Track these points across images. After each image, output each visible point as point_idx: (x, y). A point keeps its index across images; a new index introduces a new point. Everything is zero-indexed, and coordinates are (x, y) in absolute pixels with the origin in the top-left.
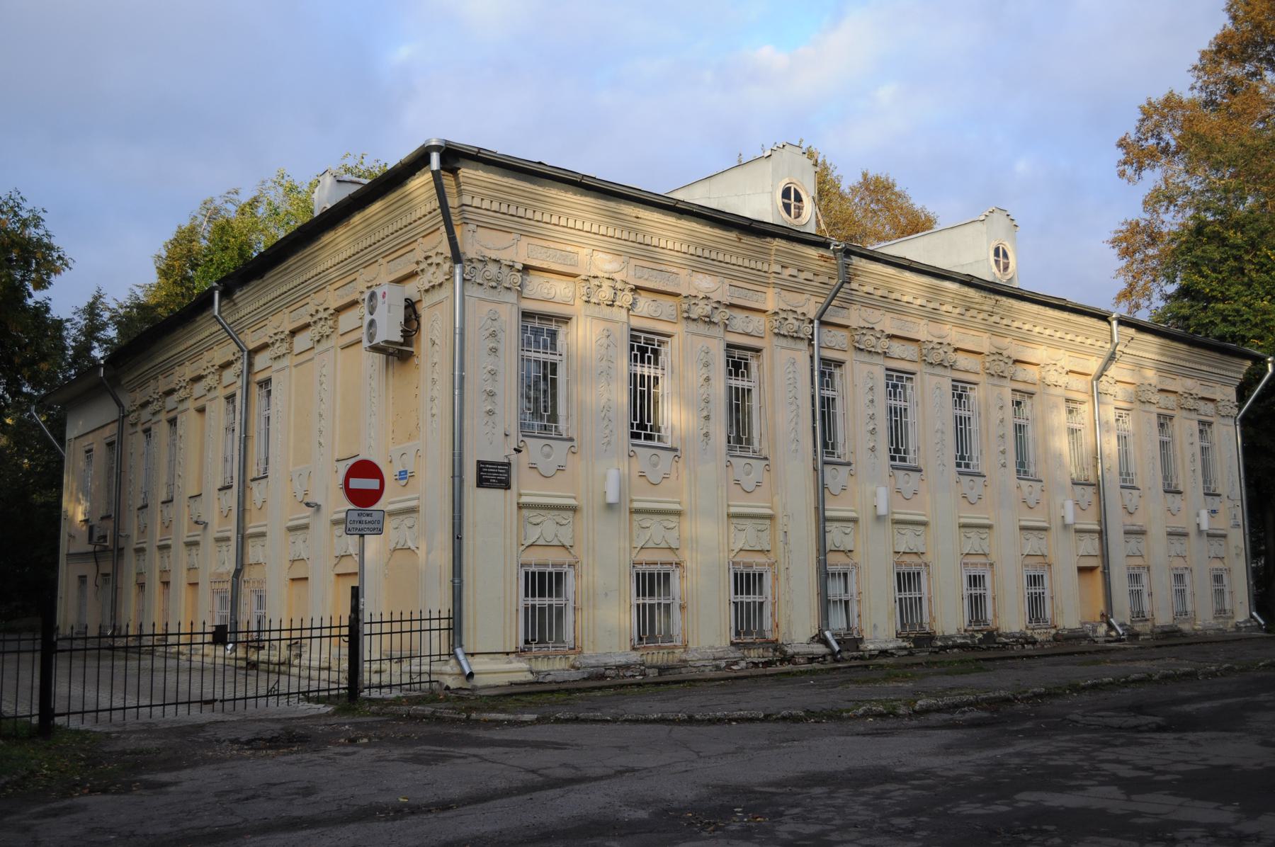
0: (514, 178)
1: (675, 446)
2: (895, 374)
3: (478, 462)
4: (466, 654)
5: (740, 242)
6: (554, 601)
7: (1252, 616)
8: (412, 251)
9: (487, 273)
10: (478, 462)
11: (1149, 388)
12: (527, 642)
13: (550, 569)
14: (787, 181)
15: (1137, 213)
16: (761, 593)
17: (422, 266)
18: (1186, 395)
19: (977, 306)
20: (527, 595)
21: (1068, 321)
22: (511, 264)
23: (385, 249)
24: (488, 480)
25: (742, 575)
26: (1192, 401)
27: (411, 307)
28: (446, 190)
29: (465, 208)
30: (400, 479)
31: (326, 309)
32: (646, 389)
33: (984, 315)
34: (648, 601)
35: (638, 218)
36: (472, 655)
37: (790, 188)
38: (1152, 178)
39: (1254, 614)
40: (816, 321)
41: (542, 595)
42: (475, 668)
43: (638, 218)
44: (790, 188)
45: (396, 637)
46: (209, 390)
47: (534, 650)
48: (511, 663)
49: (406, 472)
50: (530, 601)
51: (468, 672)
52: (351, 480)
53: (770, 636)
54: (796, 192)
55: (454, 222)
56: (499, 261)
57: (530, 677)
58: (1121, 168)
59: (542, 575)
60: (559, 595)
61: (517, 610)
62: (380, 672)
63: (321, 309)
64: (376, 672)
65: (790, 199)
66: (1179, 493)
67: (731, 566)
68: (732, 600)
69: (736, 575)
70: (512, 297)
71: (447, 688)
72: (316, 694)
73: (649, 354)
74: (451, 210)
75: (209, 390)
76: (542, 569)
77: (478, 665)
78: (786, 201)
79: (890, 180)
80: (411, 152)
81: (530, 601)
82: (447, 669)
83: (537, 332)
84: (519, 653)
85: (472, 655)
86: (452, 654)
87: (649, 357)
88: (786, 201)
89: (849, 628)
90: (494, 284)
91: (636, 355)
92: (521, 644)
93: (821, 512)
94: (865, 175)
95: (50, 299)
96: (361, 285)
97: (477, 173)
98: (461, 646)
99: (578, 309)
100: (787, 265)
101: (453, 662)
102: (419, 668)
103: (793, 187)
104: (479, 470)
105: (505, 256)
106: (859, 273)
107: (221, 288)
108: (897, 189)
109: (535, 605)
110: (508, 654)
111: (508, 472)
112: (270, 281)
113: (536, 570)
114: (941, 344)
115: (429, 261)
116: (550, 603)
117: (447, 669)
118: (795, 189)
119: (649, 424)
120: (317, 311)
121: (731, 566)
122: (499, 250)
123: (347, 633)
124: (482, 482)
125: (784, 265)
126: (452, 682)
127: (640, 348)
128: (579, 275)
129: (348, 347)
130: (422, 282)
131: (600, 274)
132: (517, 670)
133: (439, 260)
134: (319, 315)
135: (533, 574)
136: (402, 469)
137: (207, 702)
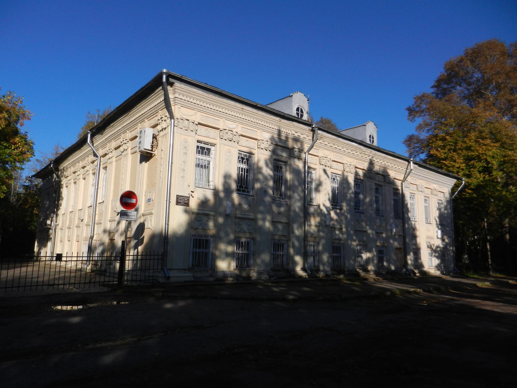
0: (195, 89)
1: (253, 195)
2: (334, 175)
3: (177, 195)
4: (168, 269)
5: (280, 122)
6: (204, 250)
7: (455, 269)
8: (157, 116)
9: (184, 124)
10: (177, 195)
11: (421, 186)
12: (193, 265)
13: (203, 238)
14: (298, 105)
15: (412, 131)
16: (283, 251)
17: (160, 121)
18: (434, 190)
19: (364, 153)
20: (194, 247)
21: (395, 160)
22: (194, 122)
23: (147, 116)
24: (180, 203)
25: (276, 244)
26: (436, 192)
27: (154, 137)
28: (169, 91)
29: (176, 98)
30: (148, 202)
31: (126, 140)
32: (243, 173)
33: (366, 156)
34: (198, 250)
35: (243, 109)
36: (171, 270)
37: (299, 108)
38: (419, 120)
39: (456, 268)
40: (307, 153)
41: (200, 248)
42: (171, 275)
43: (243, 109)
44: (299, 108)
45: (152, 261)
46: (87, 172)
47: (195, 269)
48: (185, 273)
49: (150, 199)
50: (195, 250)
51: (168, 276)
52: (124, 199)
53: (285, 267)
54: (301, 109)
55: (171, 104)
56: (188, 120)
57: (193, 279)
58: (409, 117)
59: (200, 240)
60: (206, 248)
61: (190, 253)
62: (136, 275)
63: (125, 140)
64: (135, 275)
65: (299, 111)
66: (431, 224)
67: (272, 241)
68: (272, 253)
69: (274, 244)
70: (193, 134)
71: (159, 282)
72: (107, 283)
73: (245, 160)
74: (170, 99)
75: (87, 172)
76: (200, 238)
77: (172, 274)
78: (297, 112)
79: (330, 120)
80: (155, 75)
81: (195, 250)
82: (160, 275)
83: (203, 148)
84: (189, 270)
85: (171, 270)
86: (162, 269)
87: (245, 161)
88: (297, 112)
89: (136, 279)
90: (187, 129)
91: (240, 160)
92: (190, 266)
93: (364, 153)
94: (321, 118)
95: (27, 133)
96: (138, 130)
97: (181, 85)
98: (166, 266)
99: (217, 141)
100: (297, 132)
101: (162, 272)
102: (37, 279)
103: (300, 107)
104: (177, 198)
105: (191, 119)
106: (323, 137)
107: (91, 133)
108: (332, 123)
109: (197, 252)
110: (185, 270)
111: (188, 200)
112: (108, 130)
113: (198, 238)
114: (350, 165)
115: (162, 119)
116: (203, 251)
117: (160, 275)
118: (301, 108)
119: (244, 186)
120: (123, 141)
121: (272, 241)
122: (189, 116)
123: (63, 258)
124: (178, 203)
125: (296, 131)
126: (161, 280)
127: (242, 158)
128: (220, 129)
129: (135, 153)
130: (159, 128)
131: (227, 129)
132: (188, 276)
133: (166, 118)
134: (123, 142)
135: (197, 239)
136: (149, 198)
137: (51, 285)
